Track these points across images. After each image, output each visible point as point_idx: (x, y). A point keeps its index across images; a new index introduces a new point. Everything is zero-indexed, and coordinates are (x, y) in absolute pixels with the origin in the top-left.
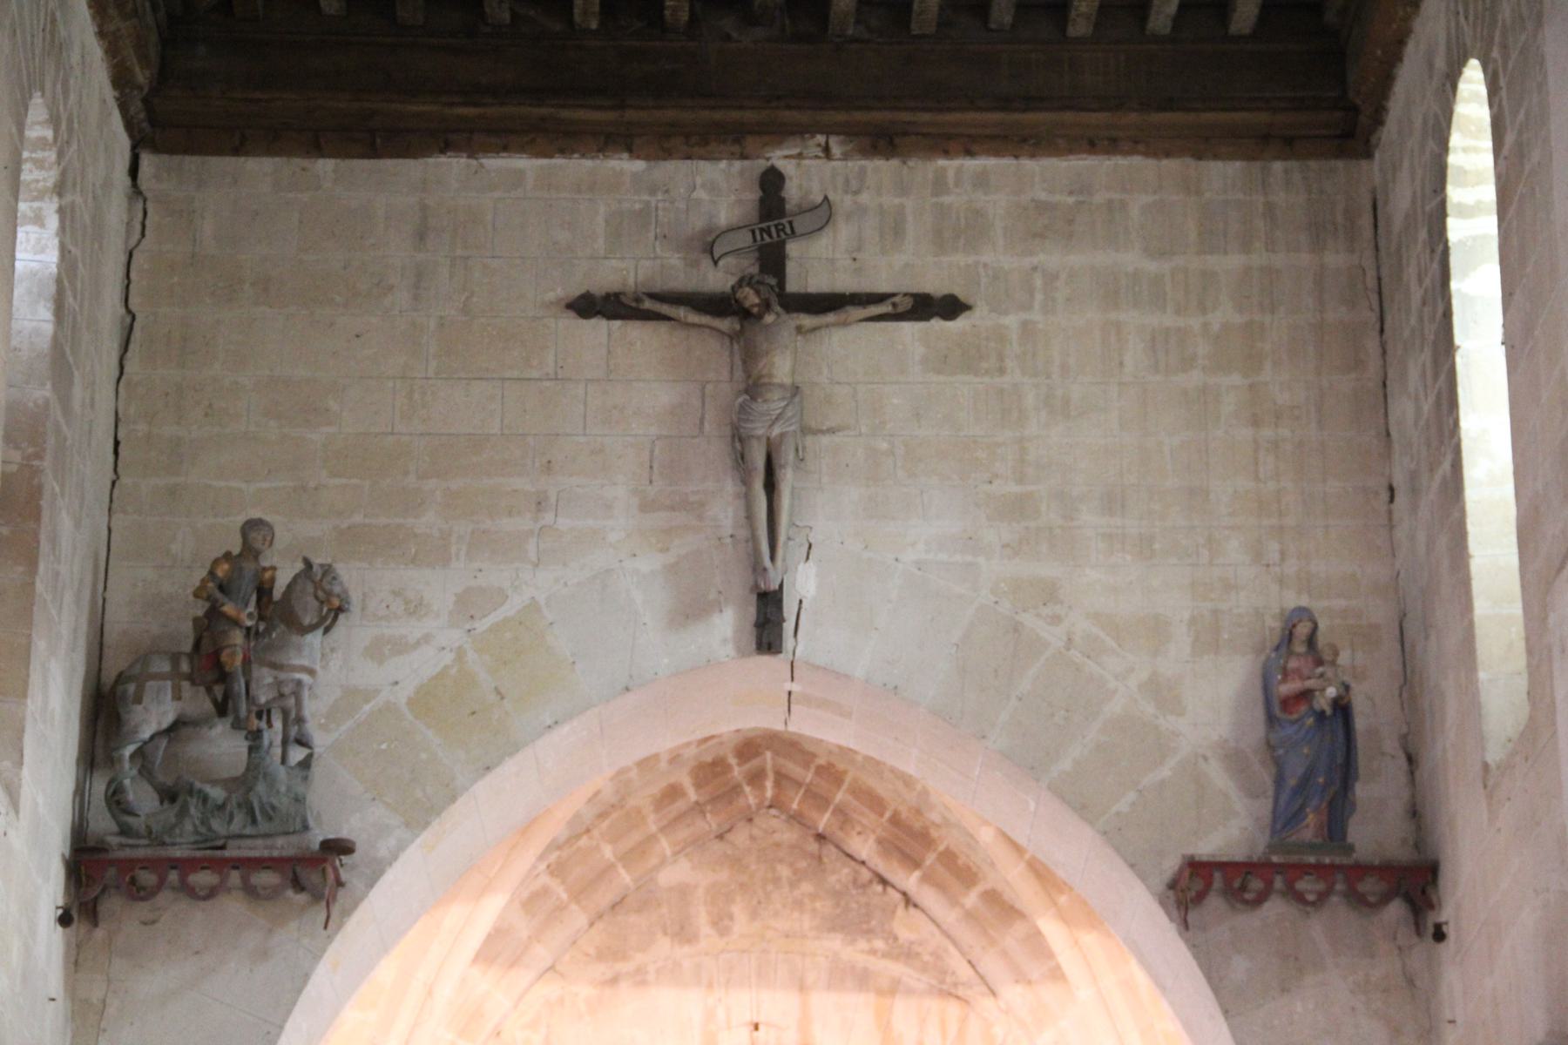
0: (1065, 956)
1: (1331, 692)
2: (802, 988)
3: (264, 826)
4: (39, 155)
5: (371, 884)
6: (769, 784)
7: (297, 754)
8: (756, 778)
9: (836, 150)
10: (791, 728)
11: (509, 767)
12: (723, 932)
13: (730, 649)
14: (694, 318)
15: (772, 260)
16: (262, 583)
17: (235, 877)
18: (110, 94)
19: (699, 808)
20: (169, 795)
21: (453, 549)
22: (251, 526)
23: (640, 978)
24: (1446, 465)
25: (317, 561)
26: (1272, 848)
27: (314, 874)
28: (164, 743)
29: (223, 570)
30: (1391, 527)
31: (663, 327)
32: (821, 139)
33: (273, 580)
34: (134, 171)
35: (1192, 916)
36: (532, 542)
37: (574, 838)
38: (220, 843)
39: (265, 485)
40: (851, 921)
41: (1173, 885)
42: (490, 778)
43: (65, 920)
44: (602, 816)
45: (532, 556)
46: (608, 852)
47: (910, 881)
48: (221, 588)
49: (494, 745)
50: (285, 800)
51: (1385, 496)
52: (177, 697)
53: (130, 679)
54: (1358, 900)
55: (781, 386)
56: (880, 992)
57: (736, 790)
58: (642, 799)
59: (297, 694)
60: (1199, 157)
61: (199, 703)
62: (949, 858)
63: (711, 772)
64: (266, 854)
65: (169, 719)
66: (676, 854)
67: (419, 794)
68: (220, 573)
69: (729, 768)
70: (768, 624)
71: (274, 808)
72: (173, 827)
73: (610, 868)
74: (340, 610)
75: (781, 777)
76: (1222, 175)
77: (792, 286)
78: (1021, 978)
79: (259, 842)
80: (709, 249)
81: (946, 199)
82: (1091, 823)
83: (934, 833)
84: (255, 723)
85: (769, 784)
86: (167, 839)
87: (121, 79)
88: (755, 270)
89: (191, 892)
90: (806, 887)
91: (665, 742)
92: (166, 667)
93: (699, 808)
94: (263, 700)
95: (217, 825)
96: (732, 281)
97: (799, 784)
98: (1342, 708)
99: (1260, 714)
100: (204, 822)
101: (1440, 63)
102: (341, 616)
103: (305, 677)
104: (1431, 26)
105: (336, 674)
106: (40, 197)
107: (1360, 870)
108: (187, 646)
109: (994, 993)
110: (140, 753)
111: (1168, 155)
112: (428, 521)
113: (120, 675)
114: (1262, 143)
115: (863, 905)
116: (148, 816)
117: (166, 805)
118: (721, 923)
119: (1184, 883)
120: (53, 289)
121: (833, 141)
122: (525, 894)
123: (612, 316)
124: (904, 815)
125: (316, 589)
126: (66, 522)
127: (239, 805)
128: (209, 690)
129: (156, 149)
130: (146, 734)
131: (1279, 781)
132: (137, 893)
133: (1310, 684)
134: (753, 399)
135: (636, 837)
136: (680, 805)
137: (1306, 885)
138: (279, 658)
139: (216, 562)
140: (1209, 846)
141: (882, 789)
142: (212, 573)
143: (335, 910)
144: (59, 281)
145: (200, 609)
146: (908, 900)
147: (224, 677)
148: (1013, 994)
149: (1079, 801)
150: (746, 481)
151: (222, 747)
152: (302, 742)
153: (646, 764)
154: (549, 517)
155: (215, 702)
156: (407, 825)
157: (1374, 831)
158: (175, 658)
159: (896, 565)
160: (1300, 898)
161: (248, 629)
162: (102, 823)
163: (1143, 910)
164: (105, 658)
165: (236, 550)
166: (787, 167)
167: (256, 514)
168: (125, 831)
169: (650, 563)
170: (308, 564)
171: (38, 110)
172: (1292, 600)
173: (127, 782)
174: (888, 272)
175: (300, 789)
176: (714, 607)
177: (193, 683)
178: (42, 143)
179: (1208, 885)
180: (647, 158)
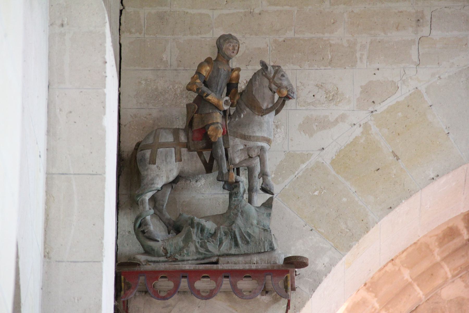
3: (243, 248)
7: (260, 198)
16: (231, 80)
17: (226, 283)
20: (175, 228)
21: (358, 55)
22: (223, 40)
25: (270, 63)
29: (206, 70)
33: (238, 77)
36: (414, 49)
38: (214, 259)
39: (225, 12)
42: (392, 215)
45: (415, 58)
50: (257, 230)
52: (179, 159)
53: (147, 147)
61: (193, 162)
64: (247, 267)
66: (453, 276)
67: (343, 227)
68: (204, 73)
71: (249, 235)
72: (181, 249)
73: (409, 285)
74: (288, 97)
79: (241, 259)
86: (179, 258)
89: (197, 293)
92: (170, 138)
94: (237, 161)
95: (212, 247)
102: (288, 102)
103: (264, 144)
105: (284, 141)
108: (181, 123)
110: (153, 199)
112: (339, 35)
113: (138, 144)
116: (163, 241)
117: (173, 233)
125: (270, 83)
127: (226, 234)
128: (200, 154)
135: (425, 264)
138: (245, 132)
139: (201, 65)
142: (198, 73)
147: (210, 145)
151: (207, 195)
154: (425, 31)
155: (204, 162)
156: (336, 248)
158: (176, 132)
161: (225, 112)
164: (121, 131)
165: (214, 58)
167: (220, 32)
168: (148, 251)
173: (148, 218)
175: (266, 222)
177: (189, 150)
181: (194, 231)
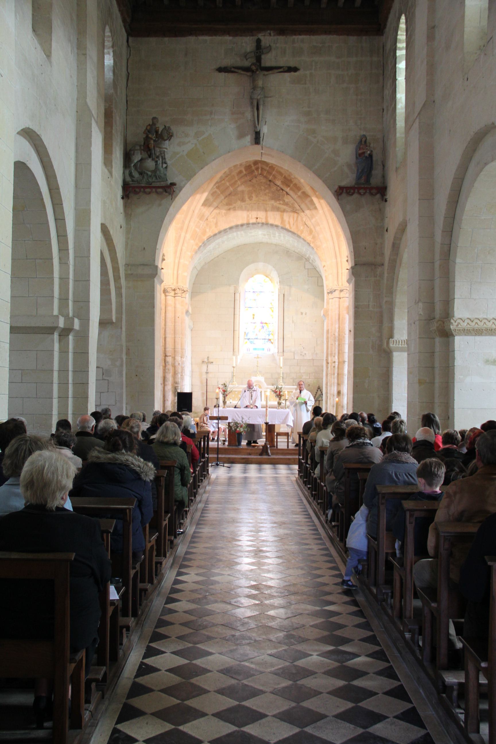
0: (317, 205)
1: (369, 152)
2: (266, 211)
4: (108, 39)
5: (180, 191)
6: (260, 170)
7: (165, 166)
8: (257, 169)
9: (272, 34)
10: (263, 160)
11: (206, 168)
12: (251, 200)
13: (250, 144)
14: (242, 72)
15: (259, 59)
17: (154, 190)
18: (122, 24)
19: (246, 175)
20: (141, 173)
23: (235, 209)
24: (393, 105)
25: (167, 125)
26: (356, 184)
27: (168, 190)
28: (139, 163)
29: (148, 128)
30: (383, 117)
31: (236, 74)
32: (269, 31)
33: (158, 130)
34: (128, 41)
35: (339, 197)
37: (221, 181)
40: (276, 198)
41: (336, 191)
42: (202, 170)
43: (123, 198)
44: (227, 177)
45: (210, 124)
46: (228, 184)
47: (288, 190)
48: (149, 131)
49: (203, 164)
51: (382, 111)
52: (141, 154)
54: (371, 194)
55: (260, 87)
56: (281, 212)
57: (253, 171)
58: (234, 173)
59: (164, 153)
60: (348, 35)
61: (145, 155)
62: (295, 185)
63: (248, 168)
65: (140, 158)
69: (251, 167)
70: (257, 139)
74: (172, 136)
75: (262, 169)
76: (352, 39)
77: (263, 65)
78: (309, 209)
80: (245, 56)
81: (295, 45)
82: (321, 179)
83: (292, 180)
84: (156, 159)
85: (260, 170)
87: (124, 21)
88: (255, 61)
89: (145, 192)
90: (267, 191)
91: (238, 163)
93: (246, 175)
94: (157, 154)
95: (150, 180)
96: (250, 64)
97: (266, 170)
98: (371, 156)
99: (355, 157)
100: (148, 179)
101: (397, 15)
103: (165, 150)
104: (396, 6)
106: (109, 48)
107: (371, 189)
108: (142, 144)
109: (303, 212)
110: (135, 165)
111: (341, 35)
114: (361, 32)
115: (278, 195)
118: (250, 198)
119: (338, 191)
120: (112, 69)
121: (272, 32)
122: (212, 192)
123: (225, 72)
124: (287, 176)
126: (118, 118)
128: (147, 152)
129: (132, 36)
130: (136, 162)
131: (358, 170)
132: (136, 193)
133: (364, 151)
134: (254, 90)
135: (233, 181)
136: (242, 174)
137: (362, 191)
139: (147, 126)
140: (344, 184)
141: (282, 171)
142: (146, 128)
143: (173, 196)
144: (114, 67)
145: (145, 136)
146: (287, 194)
148: (307, 212)
149: (319, 174)
150: (253, 108)
151: (150, 164)
152: (166, 163)
153: (235, 166)
157: (375, 181)
158: (140, 146)
159: (281, 126)
160: (360, 194)
162: (128, 179)
163: (330, 195)
165: (151, 124)
166: (262, 38)
167: (154, 116)
169: (233, 126)
170: (165, 126)
171: (107, 29)
172: (363, 133)
174: (283, 62)
176: (247, 135)
178: (108, 37)
179: (343, 191)
180: (233, 36)
181: (145, 175)
